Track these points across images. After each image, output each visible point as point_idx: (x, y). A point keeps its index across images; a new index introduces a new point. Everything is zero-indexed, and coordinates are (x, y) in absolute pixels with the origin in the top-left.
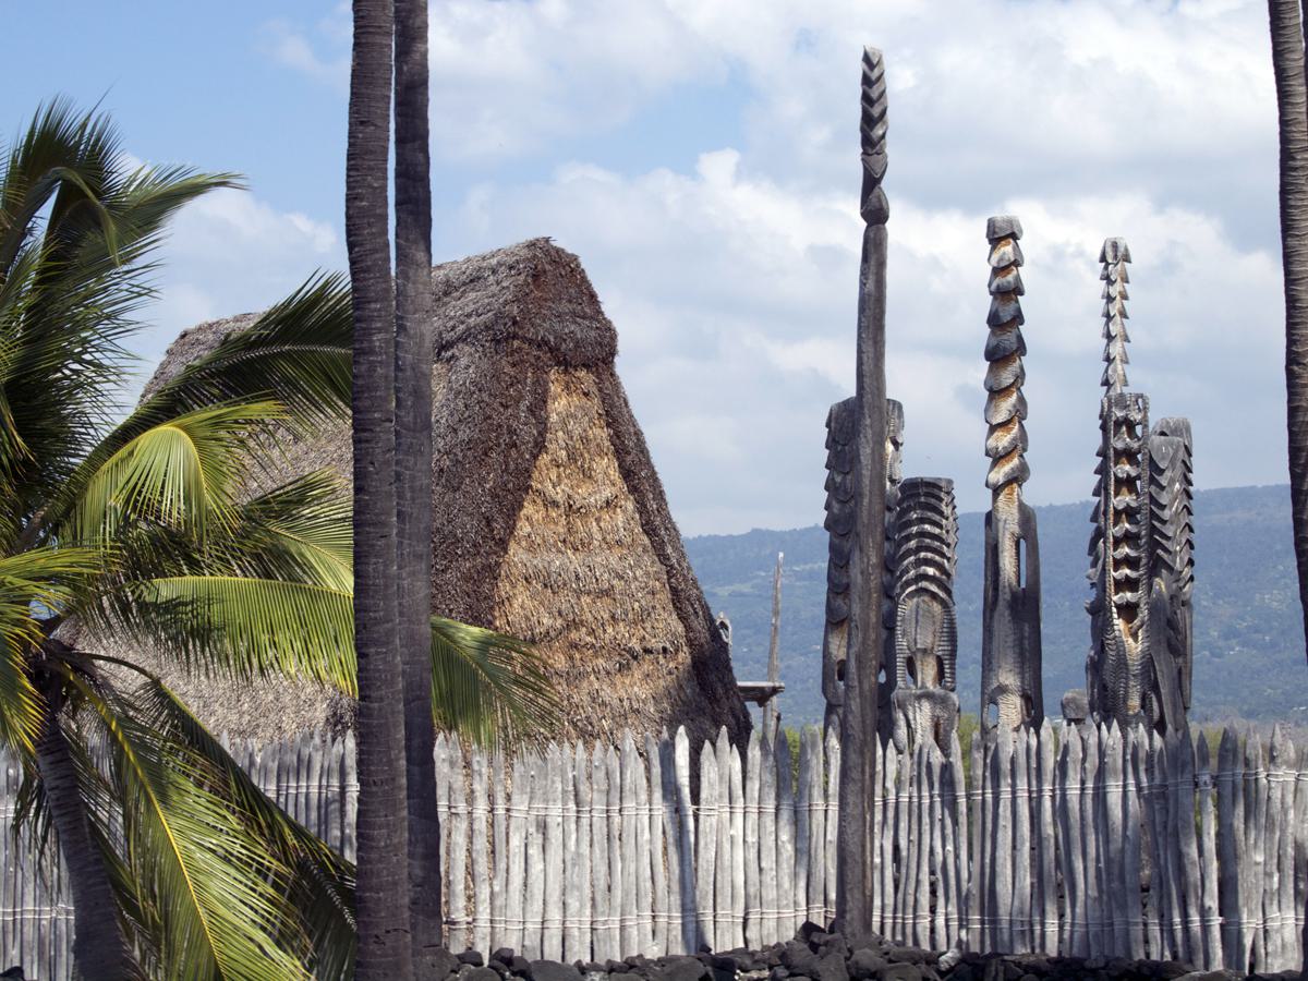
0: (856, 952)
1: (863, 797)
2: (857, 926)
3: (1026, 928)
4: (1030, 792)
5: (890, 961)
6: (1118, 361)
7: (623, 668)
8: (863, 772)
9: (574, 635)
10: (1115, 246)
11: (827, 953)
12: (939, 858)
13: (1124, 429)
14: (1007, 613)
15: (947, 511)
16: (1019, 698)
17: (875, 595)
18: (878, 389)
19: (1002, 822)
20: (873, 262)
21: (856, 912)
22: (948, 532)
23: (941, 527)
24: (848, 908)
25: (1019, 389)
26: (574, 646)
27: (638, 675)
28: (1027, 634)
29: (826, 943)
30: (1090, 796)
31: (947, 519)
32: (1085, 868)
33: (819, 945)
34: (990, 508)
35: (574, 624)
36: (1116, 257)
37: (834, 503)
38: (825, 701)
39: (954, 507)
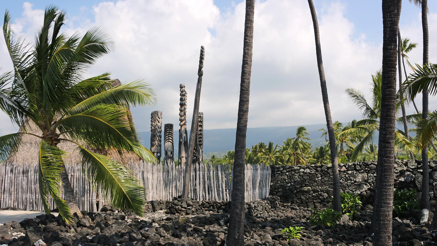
34: (180, 128)
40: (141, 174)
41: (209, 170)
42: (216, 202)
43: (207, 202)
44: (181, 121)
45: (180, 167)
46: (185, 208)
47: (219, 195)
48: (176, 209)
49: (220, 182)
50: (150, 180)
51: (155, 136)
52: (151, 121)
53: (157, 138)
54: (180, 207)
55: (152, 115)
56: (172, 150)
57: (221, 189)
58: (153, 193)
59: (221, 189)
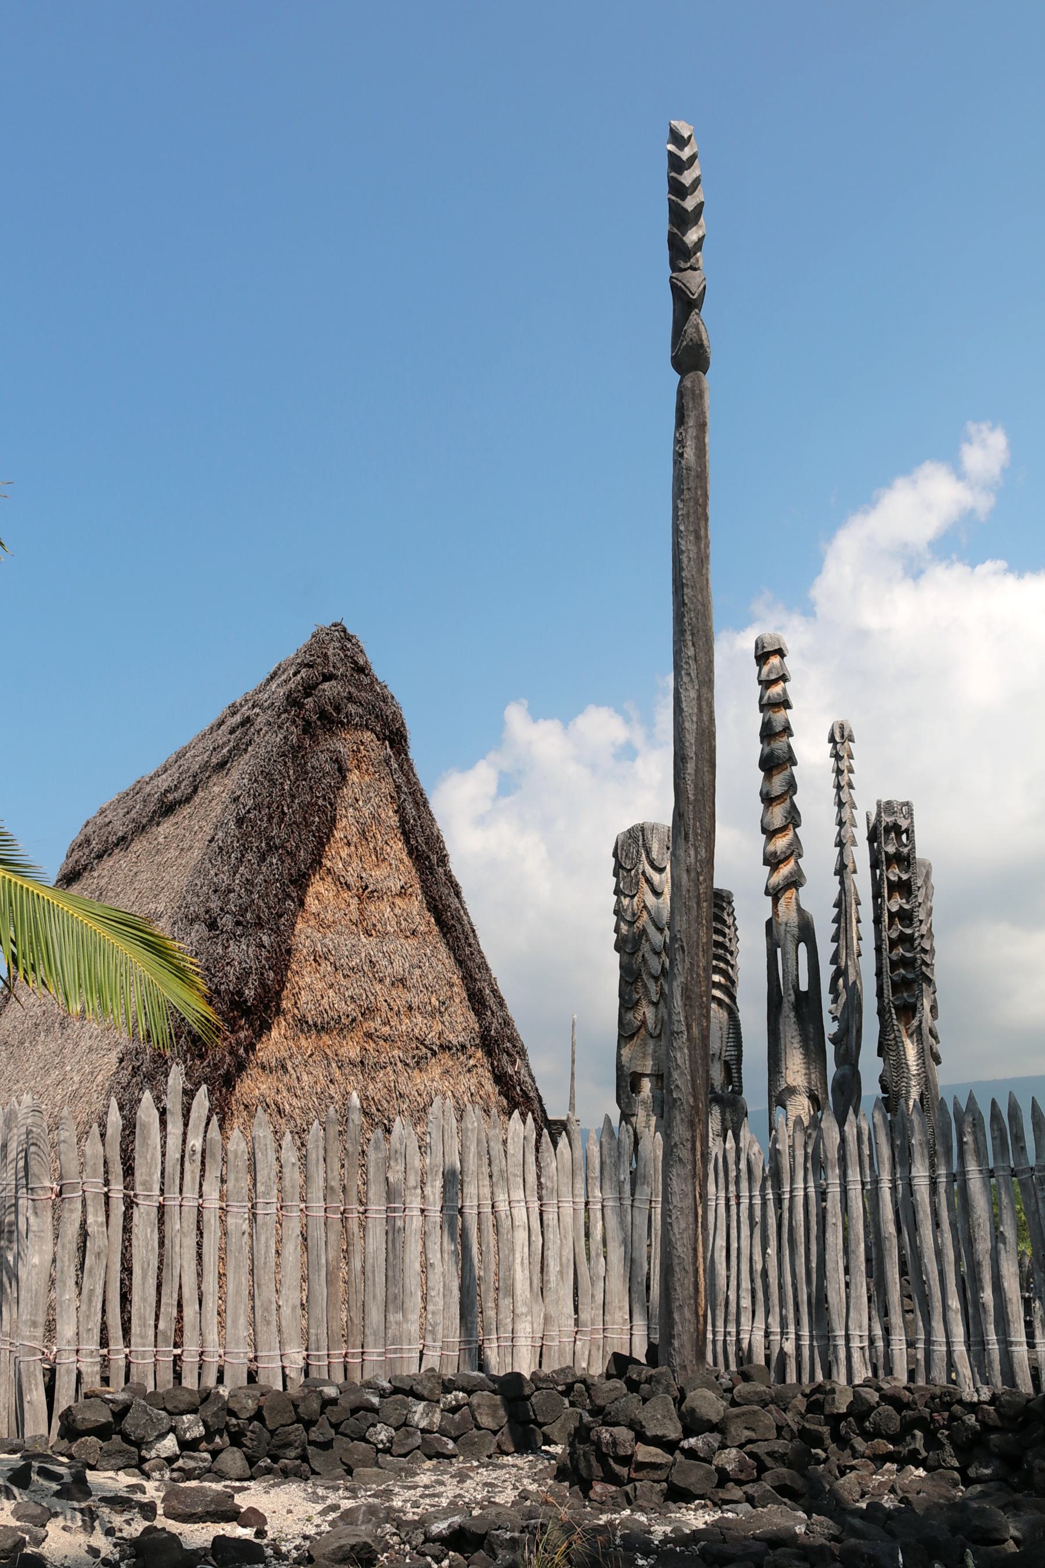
0: (690, 1395)
1: (694, 1183)
2: (689, 1354)
3: (866, 1344)
4: (863, 1184)
5: (734, 1403)
6: (848, 824)
7: (420, 1063)
8: (694, 1149)
9: (370, 1026)
10: (842, 728)
11: (653, 1394)
12: (758, 1267)
13: (893, 835)
14: (792, 1015)
15: (729, 921)
16: (807, 1099)
17: (705, 904)
18: (703, 605)
19: (831, 1220)
20: (691, 422)
21: (685, 1337)
22: (730, 940)
23: (724, 935)
24: (676, 1332)
25: (791, 798)
26: (369, 1035)
27: (437, 1071)
28: (811, 1035)
29: (649, 1380)
30: (944, 1184)
31: (729, 928)
32: (942, 1273)
33: (640, 1383)
34: (769, 915)
35: (368, 1012)
36: (842, 736)
37: (622, 924)
38: (619, 1111)
40: (435, 1189)
41: (902, 1157)
42: (947, 1400)
43: (886, 1398)
44: (773, 861)
45: (730, 1144)
46: (670, 1446)
47: (976, 1343)
48: (598, 1444)
49: (983, 1246)
50: (521, 1236)
51: (639, 976)
52: (617, 892)
53: (652, 987)
54: (624, 1434)
55: (615, 854)
56: (729, 1053)
57: (987, 1296)
58: (547, 1319)
59: (987, 1296)
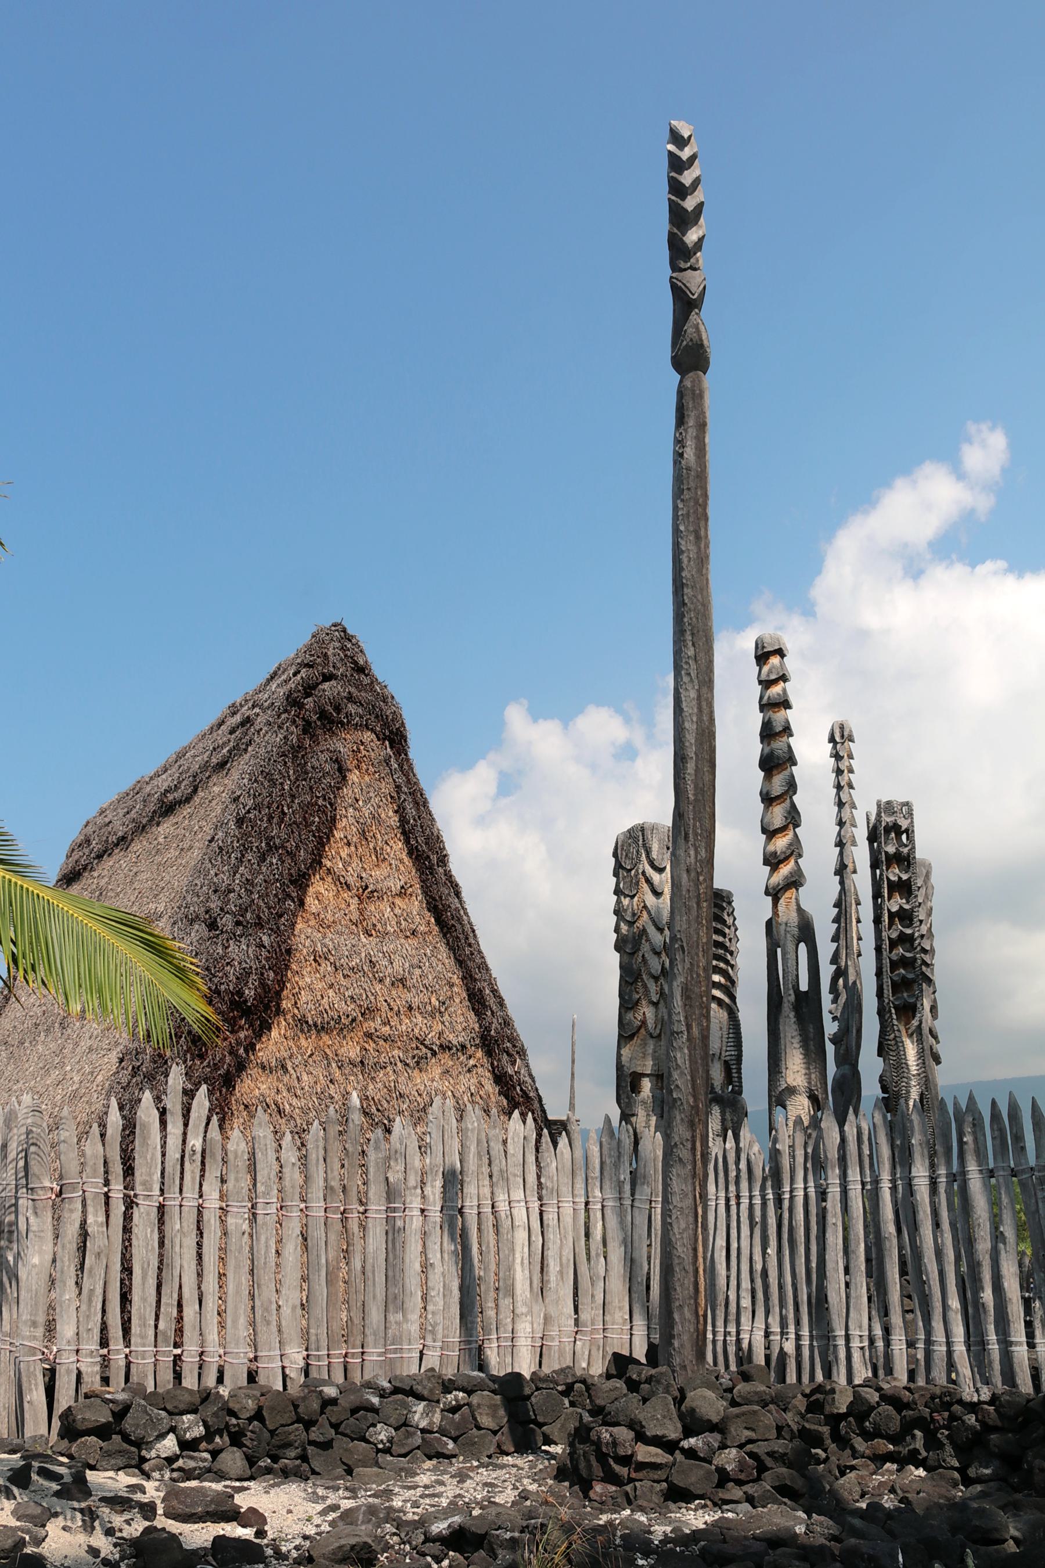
0: (690, 1395)
1: (694, 1183)
2: (689, 1354)
3: (866, 1344)
4: (863, 1184)
5: (734, 1403)
6: (848, 824)
7: (420, 1063)
8: (694, 1149)
9: (370, 1026)
10: (842, 728)
11: (653, 1394)
12: (758, 1267)
13: (893, 835)
14: (792, 1015)
15: (729, 921)
16: (807, 1099)
17: (705, 904)
18: (703, 605)
19: (831, 1220)
20: (691, 422)
21: (685, 1337)
22: (730, 940)
23: (724, 935)
24: (676, 1332)
25: (791, 798)
26: (369, 1035)
27: (437, 1071)
28: (811, 1035)
29: (649, 1380)
30: (944, 1184)
31: (729, 928)
32: (942, 1273)
33: (640, 1383)
34: (769, 915)
35: (368, 1012)
36: (842, 736)
37: (622, 924)
38: (619, 1111)
39: (736, 930)
40: (435, 1189)
41: (902, 1157)
42: (947, 1400)
43: (886, 1398)
44: (773, 861)
45: (730, 1144)
46: (670, 1446)
47: (976, 1343)
48: (598, 1444)
49: (983, 1246)
50: (521, 1236)
51: (639, 976)
52: (617, 892)
53: (652, 987)
54: (624, 1434)
55: (615, 854)
56: (729, 1053)
57: (987, 1296)
58: (547, 1319)
59: (987, 1296)
